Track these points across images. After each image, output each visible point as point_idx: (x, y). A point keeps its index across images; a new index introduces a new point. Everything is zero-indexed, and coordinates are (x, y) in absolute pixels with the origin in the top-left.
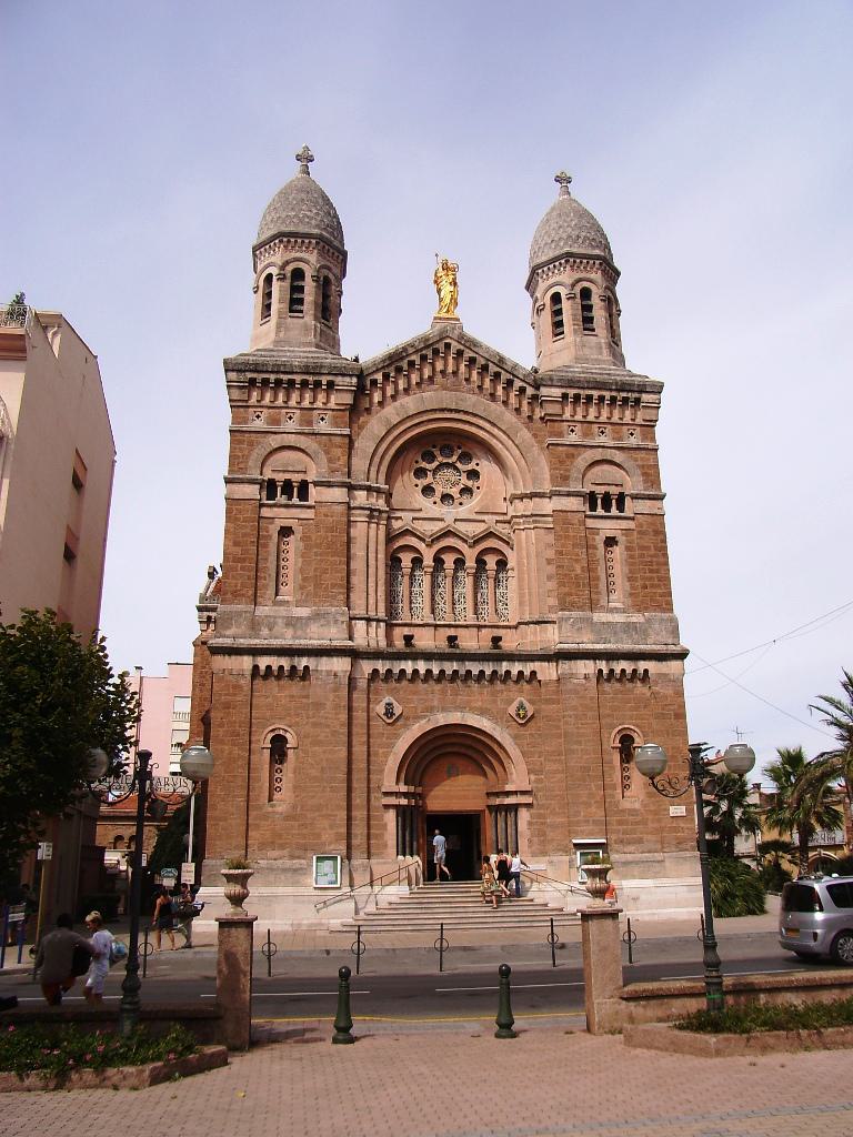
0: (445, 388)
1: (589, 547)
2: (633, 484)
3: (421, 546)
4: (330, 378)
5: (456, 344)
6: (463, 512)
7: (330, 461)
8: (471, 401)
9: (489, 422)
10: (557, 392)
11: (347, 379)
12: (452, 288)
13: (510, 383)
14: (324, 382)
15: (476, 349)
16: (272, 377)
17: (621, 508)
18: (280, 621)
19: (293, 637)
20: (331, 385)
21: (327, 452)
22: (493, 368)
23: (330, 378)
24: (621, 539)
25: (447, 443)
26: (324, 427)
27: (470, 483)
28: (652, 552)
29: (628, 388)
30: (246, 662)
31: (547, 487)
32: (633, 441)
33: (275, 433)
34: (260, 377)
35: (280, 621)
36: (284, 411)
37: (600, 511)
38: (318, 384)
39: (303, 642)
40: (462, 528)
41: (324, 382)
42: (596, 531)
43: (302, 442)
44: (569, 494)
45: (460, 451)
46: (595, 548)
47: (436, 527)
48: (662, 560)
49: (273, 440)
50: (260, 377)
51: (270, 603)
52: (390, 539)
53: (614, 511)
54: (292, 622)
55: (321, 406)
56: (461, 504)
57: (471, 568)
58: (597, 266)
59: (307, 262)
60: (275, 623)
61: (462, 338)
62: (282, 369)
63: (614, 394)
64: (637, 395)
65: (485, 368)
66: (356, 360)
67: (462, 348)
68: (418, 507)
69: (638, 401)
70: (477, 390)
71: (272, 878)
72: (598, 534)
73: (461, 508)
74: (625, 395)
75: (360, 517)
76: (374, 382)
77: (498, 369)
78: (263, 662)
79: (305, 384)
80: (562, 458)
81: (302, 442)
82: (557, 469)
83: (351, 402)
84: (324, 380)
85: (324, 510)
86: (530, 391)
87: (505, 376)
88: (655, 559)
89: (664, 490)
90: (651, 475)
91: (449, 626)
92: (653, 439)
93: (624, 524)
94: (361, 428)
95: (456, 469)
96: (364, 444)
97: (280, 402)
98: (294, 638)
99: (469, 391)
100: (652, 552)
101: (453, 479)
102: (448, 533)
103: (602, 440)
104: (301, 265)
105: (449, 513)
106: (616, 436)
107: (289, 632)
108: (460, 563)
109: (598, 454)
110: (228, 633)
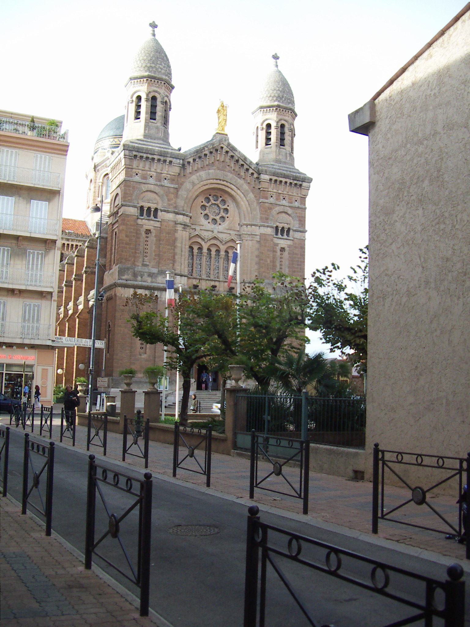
0: (218, 169)
1: (275, 251)
2: (295, 225)
3: (203, 243)
4: (171, 159)
5: (226, 147)
6: (221, 228)
7: (169, 200)
8: (230, 176)
9: (237, 187)
10: (267, 177)
11: (178, 161)
12: (291, 133)
13: (247, 170)
14: (168, 161)
15: (234, 152)
16: (145, 155)
17: (288, 235)
18: (146, 274)
19: (151, 282)
20: (171, 162)
21: (167, 196)
22: (241, 162)
23: (171, 159)
24: (287, 249)
25: (216, 194)
26: (166, 183)
27: (224, 215)
28: (299, 256)
29: (297, 179)
30: (131, 291)
31: (258, 222)
32: (296, 204)
33: (144, 183)
34: (139, 154)
35: (146, 274)
36: (149, 172)
37: (280, 236)
38: (165, 161)
39: (155, 284)
40: (220, 236)
41: (168, 161)
42: (277, 245)
43: (157, 189)
44: (268, 227)
45: (221, 199)
46: (276, 252)
47: (209, 235)
48: (302, 260)
49: (144, 187)
50: (139, 154)
51: (140, 265)
52: (190, 239)
53: (285, 237)
54: (151, 275)
55: (166, 172)
56: (220, 224)
57: (205, 253)
58: (145, 81)
59: (159, 94)
60: (144, 275)
61: (229, 145)
62: (150, 152)
63: (291, 181)
64: (300, 183)
65: (237, 161)
66: (180, 150)
67: (228, 150)
68: (202, 224)
69: (301, 185)
70: (233, 171)
71: (141, 386)
72: (278, 246)
73: (220, 227)
74: (295, 182)
75: (180, 228)
76: (189, 163)
77: (243, 163)
78: (139, 291)
79: (159, 160)
80: (266, 211)
81: (157, 189)
82: (263, 214)
83: (179, 172)
84: (168, 159)
85: (165, 224)
86: (256, 175)
87: (246, 167)
88: (300, 260)
89: (306, 229)
90: (302, 221)
91: (212, 280)
92: (305, 205)
93: (289, 242)
94: (182, 184)
95: (218, 206)
96: (182, 193)
97: (147, 168)
98: (152, 282)
99: (229, 171)
100: (299, 256)
101: (217, 211)
102: (215, 238)
103: (284, 202)
104: (156, 95)
105: (217, 228)
106: (290, 201)
107: (149, 280)
108: (218, 251)
109: (281, 209)
110: (123, 277)
